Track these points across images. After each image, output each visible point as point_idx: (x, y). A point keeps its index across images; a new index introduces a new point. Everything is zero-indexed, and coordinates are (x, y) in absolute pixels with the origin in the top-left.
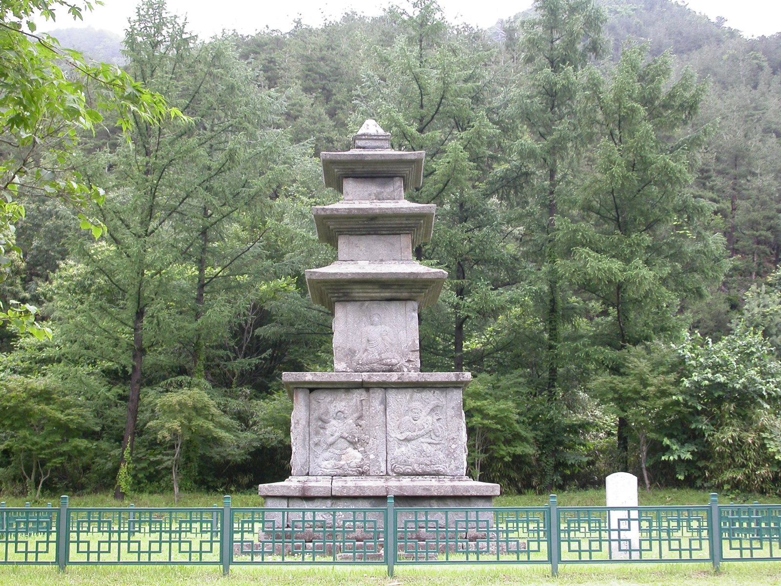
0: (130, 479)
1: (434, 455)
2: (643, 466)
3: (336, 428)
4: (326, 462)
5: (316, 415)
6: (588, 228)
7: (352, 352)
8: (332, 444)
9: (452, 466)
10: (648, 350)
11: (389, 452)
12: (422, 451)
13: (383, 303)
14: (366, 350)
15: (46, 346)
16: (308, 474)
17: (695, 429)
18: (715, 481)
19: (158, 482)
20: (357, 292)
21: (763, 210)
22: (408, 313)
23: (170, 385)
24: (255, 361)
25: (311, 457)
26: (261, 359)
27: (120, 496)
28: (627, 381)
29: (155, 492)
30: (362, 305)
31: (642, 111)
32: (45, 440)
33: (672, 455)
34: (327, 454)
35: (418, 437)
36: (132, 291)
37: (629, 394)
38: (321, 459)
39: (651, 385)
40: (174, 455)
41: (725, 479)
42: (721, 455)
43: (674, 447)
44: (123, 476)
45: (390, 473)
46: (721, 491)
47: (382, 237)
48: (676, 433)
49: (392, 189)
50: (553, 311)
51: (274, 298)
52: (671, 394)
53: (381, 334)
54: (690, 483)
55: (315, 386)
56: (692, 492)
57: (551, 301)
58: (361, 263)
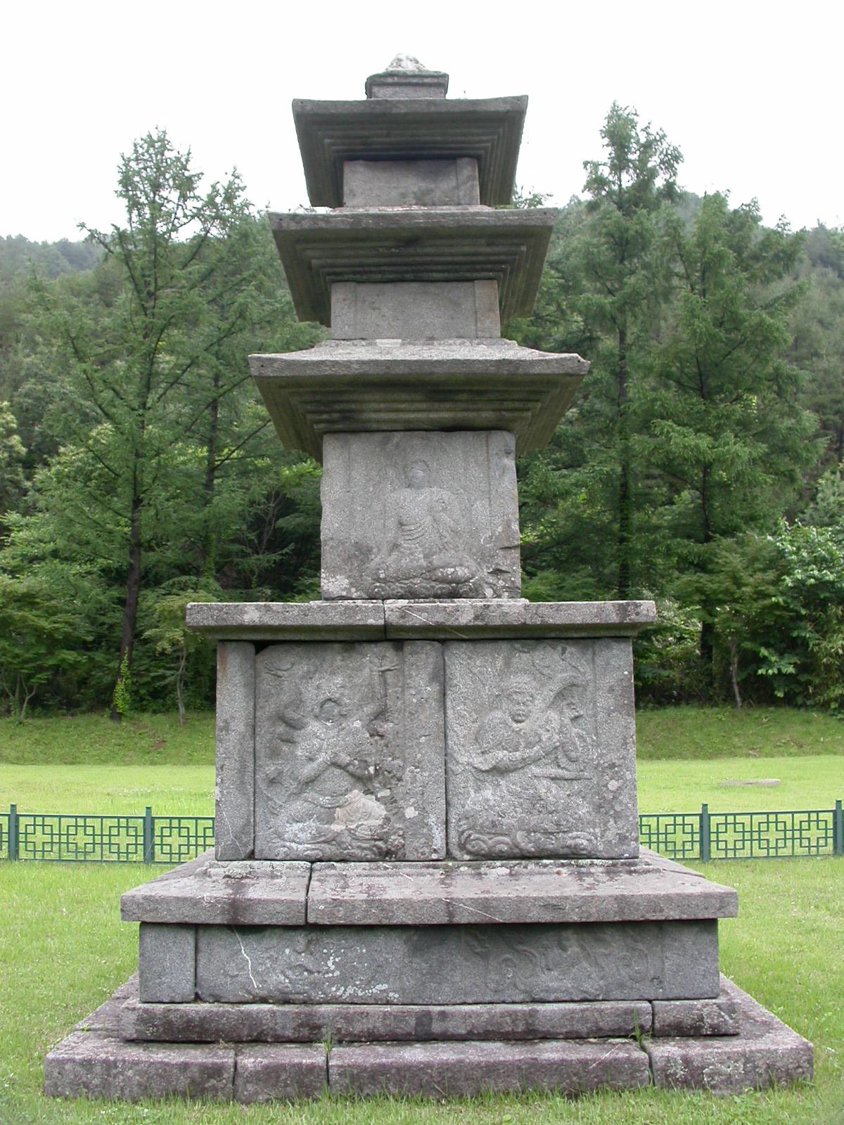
0: (128, 696)
1: (567, 807)
2: (734, 680)
3: (320, 741)
4: (296, 826)
5: (270, 708)
6: (669, 395)
7: (362, 552)
8: (310, 782)
9: (610, 835)
10: (741, 543)
11: (454, 801)
12: (536, 799)
13: (435, 437)
14: (396, 546)
16: (251, 856)
17: (798, 637)
18: (821, 699)
19: (163, 698)
20: (374, 409)
21: (830, 393)
22: (494, 460)
23: (173, 586)
24: (275, 557)
25: (259, 811)
26: (282, 555)
27: (117, 716)
28: (717, 579)
29: (160, 712)
30: (385, 442)
31: (732, 255)
32: (28, 651)
33: (771, 668)
34: (298, 806)
35: (525, 763)
36: (128, 474)
37: (720, 596)
38: (283, 817)
39: (746, 585)
40: (178, 670)
41: (833, 696)
42: (828, 667)
43: (773, 659)
44: (120, 693)
45: (456, 853)
46: (827, 710)
47: (432, 288)
48: (773, 642)
49: (453, 183)
50: (624, 497)
51: (298, 485)
52: (770, 596)
53: (431, 509)
54: (789, 701)
55: (268, 637)
56: (792, 712)
57: (622, 485)
58: (383, 343)
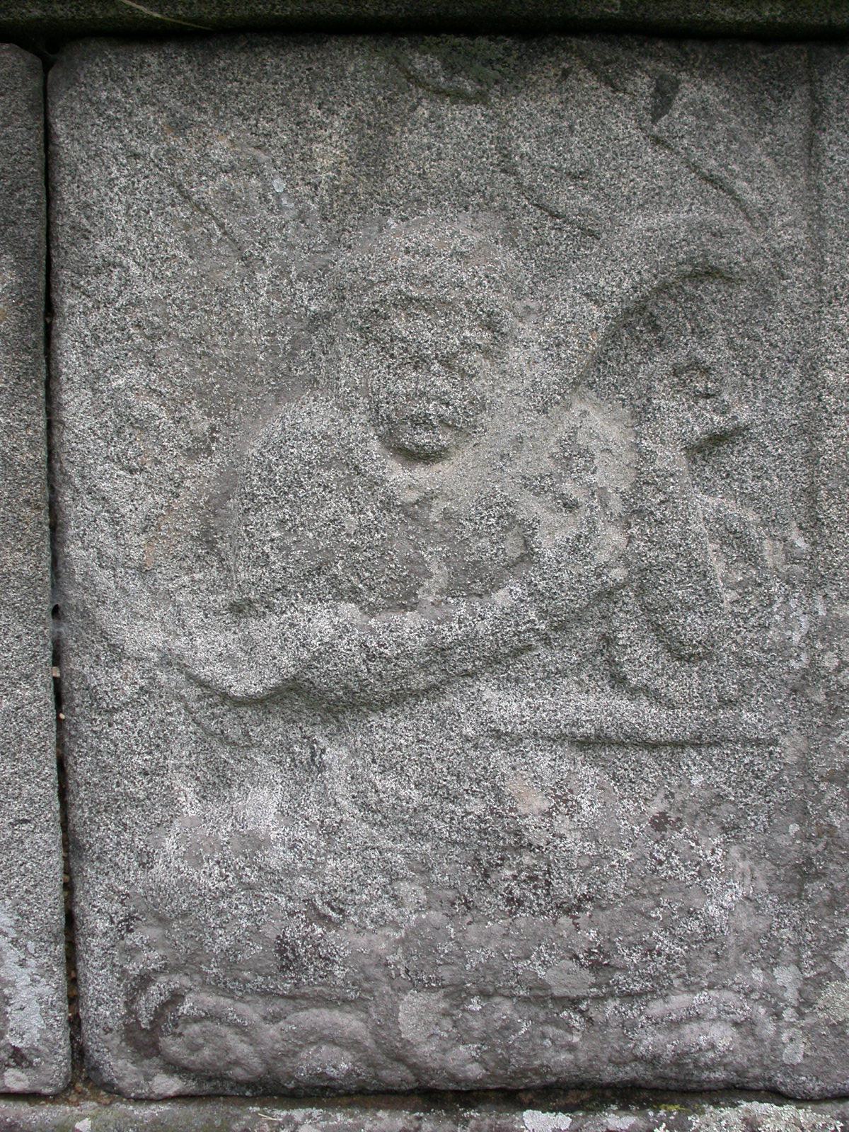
1: (649, 883)
11: (100, 832)
12: (495, 852)
15: (549, 739)
35: (447, 667)
45: (119, 1065)
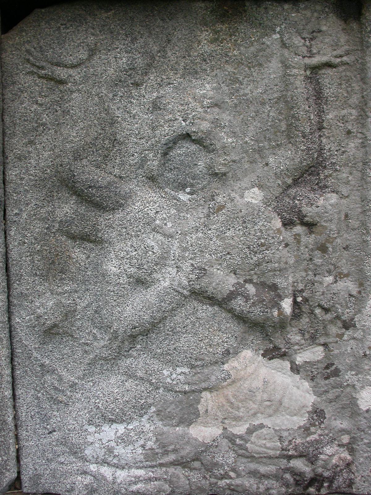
4: (110, 432)
8: (140, 335)
34: (112, 387)
